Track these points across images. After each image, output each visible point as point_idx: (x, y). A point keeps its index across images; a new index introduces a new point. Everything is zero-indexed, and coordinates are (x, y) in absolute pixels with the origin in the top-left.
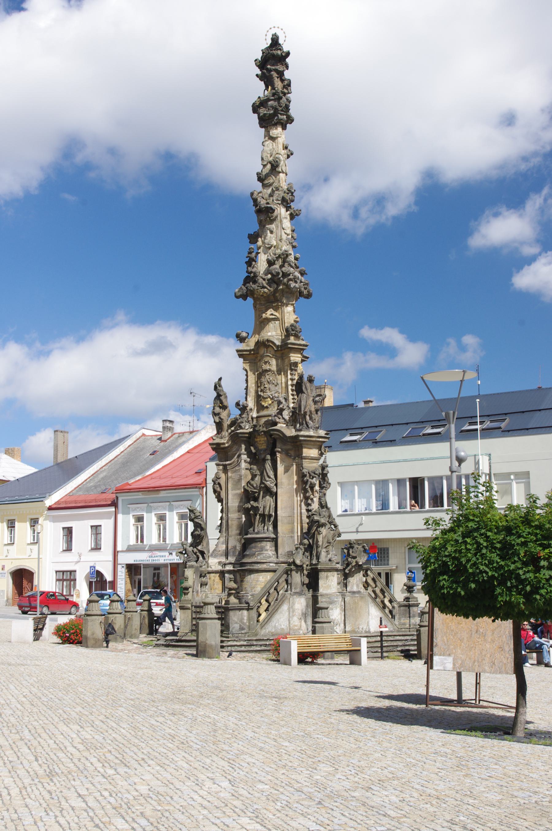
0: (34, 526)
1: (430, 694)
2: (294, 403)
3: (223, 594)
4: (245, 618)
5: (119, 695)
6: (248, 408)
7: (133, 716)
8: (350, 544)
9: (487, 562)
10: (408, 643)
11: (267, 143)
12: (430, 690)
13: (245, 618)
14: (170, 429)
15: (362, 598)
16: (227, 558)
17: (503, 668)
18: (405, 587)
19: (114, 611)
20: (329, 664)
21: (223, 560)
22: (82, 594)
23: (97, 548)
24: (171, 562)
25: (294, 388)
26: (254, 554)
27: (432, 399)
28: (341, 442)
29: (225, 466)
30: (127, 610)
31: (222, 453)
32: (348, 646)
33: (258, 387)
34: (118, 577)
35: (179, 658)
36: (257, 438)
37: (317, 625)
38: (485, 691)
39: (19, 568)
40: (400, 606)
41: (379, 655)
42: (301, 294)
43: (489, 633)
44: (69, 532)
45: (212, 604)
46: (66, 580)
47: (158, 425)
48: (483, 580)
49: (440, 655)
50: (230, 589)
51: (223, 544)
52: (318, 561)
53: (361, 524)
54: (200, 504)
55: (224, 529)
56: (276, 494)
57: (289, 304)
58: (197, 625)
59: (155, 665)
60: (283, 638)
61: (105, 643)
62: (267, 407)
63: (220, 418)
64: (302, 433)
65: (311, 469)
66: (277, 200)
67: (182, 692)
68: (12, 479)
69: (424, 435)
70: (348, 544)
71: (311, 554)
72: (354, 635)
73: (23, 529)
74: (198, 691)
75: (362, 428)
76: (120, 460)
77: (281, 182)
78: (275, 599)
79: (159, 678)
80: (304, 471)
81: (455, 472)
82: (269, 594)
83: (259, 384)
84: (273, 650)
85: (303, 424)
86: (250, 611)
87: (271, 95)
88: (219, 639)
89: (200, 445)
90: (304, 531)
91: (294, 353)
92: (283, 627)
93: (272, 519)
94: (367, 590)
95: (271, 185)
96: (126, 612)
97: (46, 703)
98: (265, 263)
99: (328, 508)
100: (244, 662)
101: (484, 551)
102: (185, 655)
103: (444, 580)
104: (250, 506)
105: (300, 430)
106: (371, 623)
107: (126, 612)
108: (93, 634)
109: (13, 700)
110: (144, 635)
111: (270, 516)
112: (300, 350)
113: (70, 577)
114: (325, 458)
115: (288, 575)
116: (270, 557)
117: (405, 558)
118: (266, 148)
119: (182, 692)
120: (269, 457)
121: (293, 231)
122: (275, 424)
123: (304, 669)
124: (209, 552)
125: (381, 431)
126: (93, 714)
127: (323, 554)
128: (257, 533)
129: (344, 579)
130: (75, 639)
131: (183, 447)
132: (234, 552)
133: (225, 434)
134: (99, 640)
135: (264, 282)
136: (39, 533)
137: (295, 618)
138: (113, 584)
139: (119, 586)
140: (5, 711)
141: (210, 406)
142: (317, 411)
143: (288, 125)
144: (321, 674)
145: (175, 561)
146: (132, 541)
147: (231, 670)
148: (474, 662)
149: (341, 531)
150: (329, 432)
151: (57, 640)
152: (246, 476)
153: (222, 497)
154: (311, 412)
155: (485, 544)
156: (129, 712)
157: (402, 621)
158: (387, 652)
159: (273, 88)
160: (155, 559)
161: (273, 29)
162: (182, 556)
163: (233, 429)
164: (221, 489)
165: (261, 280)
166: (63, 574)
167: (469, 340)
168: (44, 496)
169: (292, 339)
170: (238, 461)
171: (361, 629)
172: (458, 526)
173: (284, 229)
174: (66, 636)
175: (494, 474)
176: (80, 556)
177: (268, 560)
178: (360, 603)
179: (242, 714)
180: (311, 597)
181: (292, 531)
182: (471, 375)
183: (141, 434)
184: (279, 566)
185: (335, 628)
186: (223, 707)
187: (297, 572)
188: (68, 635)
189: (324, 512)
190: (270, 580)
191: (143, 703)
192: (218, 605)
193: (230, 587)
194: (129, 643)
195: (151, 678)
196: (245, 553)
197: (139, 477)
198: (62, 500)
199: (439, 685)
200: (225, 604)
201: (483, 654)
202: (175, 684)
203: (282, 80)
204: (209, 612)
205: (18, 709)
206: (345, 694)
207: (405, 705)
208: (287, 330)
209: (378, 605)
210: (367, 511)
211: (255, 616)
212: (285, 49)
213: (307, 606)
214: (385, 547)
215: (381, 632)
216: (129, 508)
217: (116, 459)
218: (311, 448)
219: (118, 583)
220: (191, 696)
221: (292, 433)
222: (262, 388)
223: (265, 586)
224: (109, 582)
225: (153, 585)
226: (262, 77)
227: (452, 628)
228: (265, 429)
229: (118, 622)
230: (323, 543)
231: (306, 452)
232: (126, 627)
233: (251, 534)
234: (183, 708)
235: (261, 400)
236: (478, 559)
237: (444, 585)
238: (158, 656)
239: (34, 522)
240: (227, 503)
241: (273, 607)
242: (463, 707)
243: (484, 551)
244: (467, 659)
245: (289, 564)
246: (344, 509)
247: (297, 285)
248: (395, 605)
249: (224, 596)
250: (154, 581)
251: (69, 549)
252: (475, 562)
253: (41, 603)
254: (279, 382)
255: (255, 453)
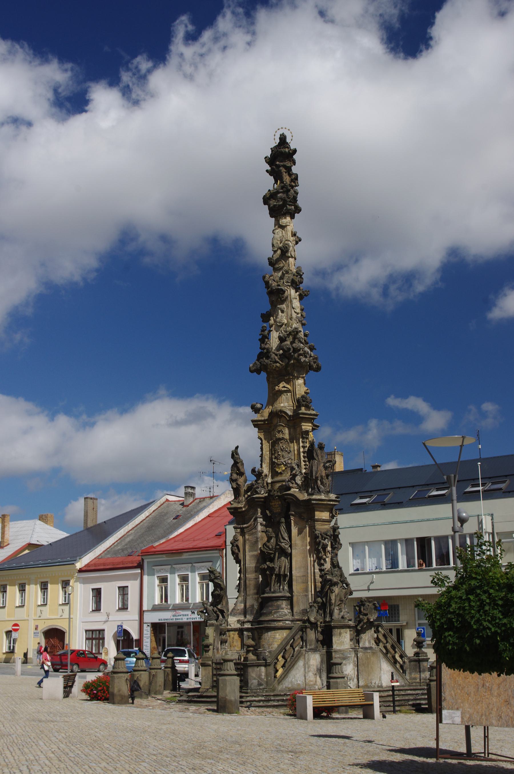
0: (65, 588)
1: (440, 747)
2: (305, 469)
3: (242, 651)
4: (263, 674)
5: (142, 751)
6: (263, 474)
7: (155, 771)
8: (361, 601)
9: (490, 619)
10: (419, 698)
11: (277, 231)
12: (440, 744)
13: (263, 674)
14: (191, 495)
15: (374, 653)
16: (245, 617)
17: (510, 722)
18: (415, 643)
19: (140, 669)
20: (344, 718)
21: (242, 618)
22: (110, 651)
23: (124, 608)
24: (194, 620)
25: (306, 455)
26: (271, 612)
27: (434, 463)
28: (352, 505)
29: (242, 529)
30: (152, 667)
31: (239, 516)
32: (362, 700)
33: (272, 454)
34: (144, 636)
35: (200, 713)
36: (272, 503)
37: (332, 680)
38: (494, 744)
39: (51, 627)
40: (411, 661)
41: (392, 709)
42: (311, 368)
43: (495, 687)
44: (97, 593)
45: (231, 661)
46: (95, 639)
47: (182, 492)
48: (487, 635)
49: (449, 709)
50: (249, 646)
51: (241, 603)
52: (331, 619)
53: (372, 583)
54: (220, 565)
55: (242, 589)
56: (291, 554)
57: (300, 377)
58: (217, 681)
59: (177, 721)
60: (299, 693)
61: (130, 699)
62: (281, 473)
63: (237, 484)
64: (314, 497)
65: (323, 531)
66: (287, 282)
67: (202, 747)
68: (45, 543)
69: (429, 497)
70: (359, 601)
71: (325, 612)
72: (367, 690)
73: (55, 590)
74: (217, 746)
75: (371, 491)
76: (146, 525)
77: (290, 266)
78: (291, 655)
79: (181, 733)
80: (317, 532)
81: (458, 532)
82: (286, 650)
83: (273, 451)
84: (289, 705)
85: (314, 488)
86: (268, 667)
87: (280, 188)
88: (238, 694)
89: (219, 509)
90: (318, 590)
91: (305, 423)
92: (299, 682)
93: (287, 579)
94: (379, 646)
95: (281, 269)
96: (150, 669)
97: (73, 759)
98: (277, 340)
99: (340, 568)
100: (263, 717)
101: (487, 608)
102: (206, 710)
103: (449, 636)
104: (266, 567)
105: (312, 494)
106: (382, 678)
107: (150, 669)
108: (119, 691)
109: (42, 756)
110: (168, 691)
111: (285, 576)
112: (310, 420)
113: (99, 636)
114: (336, 521)
115: (303, 632)
116: (286, 615)
117: (415, 615)
118: (276, 236)
119: (202, 747)
120: (283, 520)
121: (302, 310)
122: (289, 488)
123: (319, 723)
124: (228, 610)
125: (389, 494)
126: (117, 769)
127: (336, 612)
128: (273, 593)
129: (356, 636)
130: (103, 696)
131: (204, 511)
132: (252, 611)
133: (242, 498)
134: (125, 696)
135: (276, 357)
136: (69, 594)
137: (311, 674)
138: (139, 642)
139: (144, 644)
140: (34, 767)
141: (227, 472)
142: (327, 476)
143: (296, 215)
144: (335, 729)
145: (198, 620)
146: (157, 601)
147: (250, 725)
148: (482, 715)
149: (352, 589)
150: (339, 495)
151: (85, 696)
152: (262, 538)
153: (240, 558)
154: (322, 477)
155: (488, 601)
156: (151, 767)
157: (413, 675)
158: (399, 706)
159: (282, 182)
160: (178, 617)
161: (281, 129)
162: (203, 615)
163: (249, 494)
164: (239, 551)
165: (273, 356)
166: (92, 633)
167: (488, 407)
168: (75, 559)
169: (303, 410)
170: (254, 524)
171: (373, 684)
172: (462, 584)
173: (293, 308)
174: (94, 693)
175: (497, 533)
176: (108, 616)
177: (284, 618)
178: (372, 658)
179: (260, 768)
180: (325, 653)
181: (306, 590)
182: (470, 440)
183: (165, 500)
184: (294, 624)
185: (349, 683)
186: (241, 762)
187: (312, 630)
188: (95, 692)
189: (336, 571)
190: (286, 638)
191: (165, 758)
192: (238, 661)
193: (248, 644)
194: (154, 699)
195: (174, 733)
196: (262, 612)
197: (163, 541)
198: (92, 563)
199: (449, 739)
200: (244, 661)
201: (490, 707)
202: (196, 739)
203: (290, 175)
204: (229, 668)
205: (46, 765)
206: (358, 748)
207: (416, 758)
208: (298, 401)
209: (388, 660)
210: (377, 570)
211: (273, 672)
212: (292, 147)
213: (322, 662)
214: (395, 603)
215: (393, 686)
216: (154, 569)
217: (142, 524)
218: (322, 511)
219: (144, 641)
220: (211, 751)
221: (304, 496)
222: (276, 455)
223: (282, 643)
224: (135, 640)
225: (177, 643)
226: (271, 173)
227: (459, 683)
228: (279, 494)
229: (144, 678)
230: (335, 601)
231: (318, 515)
232: (150, 683)
233: (267, 593)
234: (203, 763)
235: (275, 467)
236: (481, 616)
237: (449, 640)
238: (180, 712)
239: (66, 584)
240: (245, 564)
241: (289, 664)
242: (472, 760)
243: (487, 608)
244: (475, 713)
245: (304, 621)
246: (355, 569)
247: (307, 360)
248: (406, 661)
249: (243, 652)
250: (178, 639)
251: (98, 609)
252: (479, 619)
253: (71, 661)
254: (292, 449)
255: (271, 517)
